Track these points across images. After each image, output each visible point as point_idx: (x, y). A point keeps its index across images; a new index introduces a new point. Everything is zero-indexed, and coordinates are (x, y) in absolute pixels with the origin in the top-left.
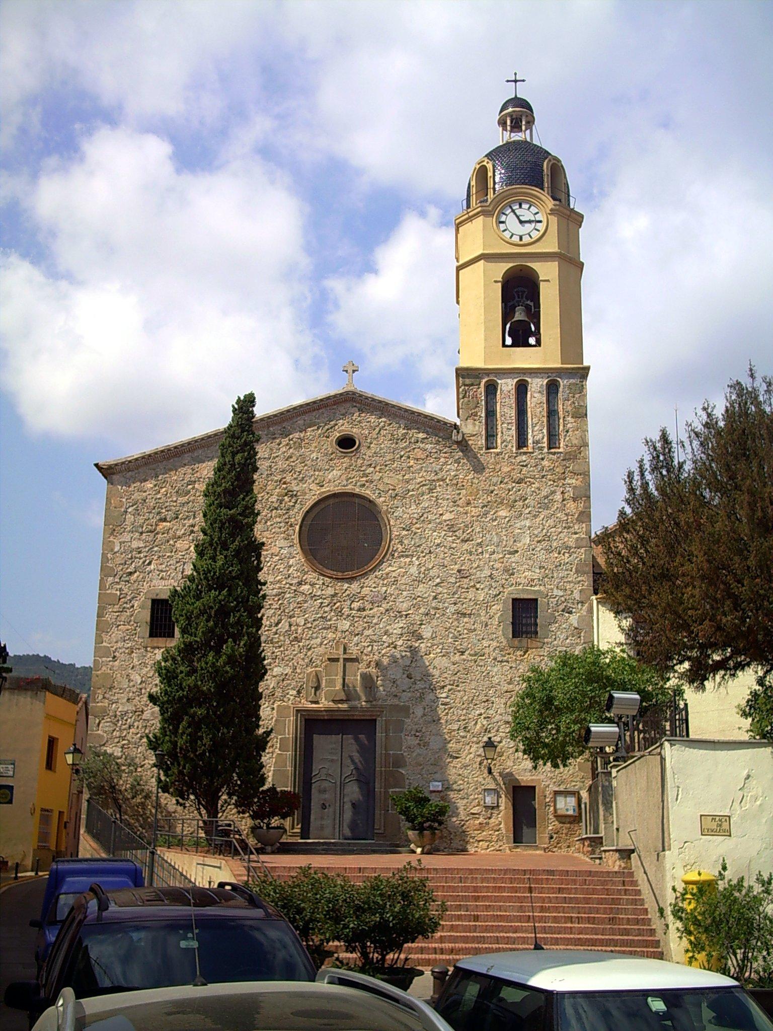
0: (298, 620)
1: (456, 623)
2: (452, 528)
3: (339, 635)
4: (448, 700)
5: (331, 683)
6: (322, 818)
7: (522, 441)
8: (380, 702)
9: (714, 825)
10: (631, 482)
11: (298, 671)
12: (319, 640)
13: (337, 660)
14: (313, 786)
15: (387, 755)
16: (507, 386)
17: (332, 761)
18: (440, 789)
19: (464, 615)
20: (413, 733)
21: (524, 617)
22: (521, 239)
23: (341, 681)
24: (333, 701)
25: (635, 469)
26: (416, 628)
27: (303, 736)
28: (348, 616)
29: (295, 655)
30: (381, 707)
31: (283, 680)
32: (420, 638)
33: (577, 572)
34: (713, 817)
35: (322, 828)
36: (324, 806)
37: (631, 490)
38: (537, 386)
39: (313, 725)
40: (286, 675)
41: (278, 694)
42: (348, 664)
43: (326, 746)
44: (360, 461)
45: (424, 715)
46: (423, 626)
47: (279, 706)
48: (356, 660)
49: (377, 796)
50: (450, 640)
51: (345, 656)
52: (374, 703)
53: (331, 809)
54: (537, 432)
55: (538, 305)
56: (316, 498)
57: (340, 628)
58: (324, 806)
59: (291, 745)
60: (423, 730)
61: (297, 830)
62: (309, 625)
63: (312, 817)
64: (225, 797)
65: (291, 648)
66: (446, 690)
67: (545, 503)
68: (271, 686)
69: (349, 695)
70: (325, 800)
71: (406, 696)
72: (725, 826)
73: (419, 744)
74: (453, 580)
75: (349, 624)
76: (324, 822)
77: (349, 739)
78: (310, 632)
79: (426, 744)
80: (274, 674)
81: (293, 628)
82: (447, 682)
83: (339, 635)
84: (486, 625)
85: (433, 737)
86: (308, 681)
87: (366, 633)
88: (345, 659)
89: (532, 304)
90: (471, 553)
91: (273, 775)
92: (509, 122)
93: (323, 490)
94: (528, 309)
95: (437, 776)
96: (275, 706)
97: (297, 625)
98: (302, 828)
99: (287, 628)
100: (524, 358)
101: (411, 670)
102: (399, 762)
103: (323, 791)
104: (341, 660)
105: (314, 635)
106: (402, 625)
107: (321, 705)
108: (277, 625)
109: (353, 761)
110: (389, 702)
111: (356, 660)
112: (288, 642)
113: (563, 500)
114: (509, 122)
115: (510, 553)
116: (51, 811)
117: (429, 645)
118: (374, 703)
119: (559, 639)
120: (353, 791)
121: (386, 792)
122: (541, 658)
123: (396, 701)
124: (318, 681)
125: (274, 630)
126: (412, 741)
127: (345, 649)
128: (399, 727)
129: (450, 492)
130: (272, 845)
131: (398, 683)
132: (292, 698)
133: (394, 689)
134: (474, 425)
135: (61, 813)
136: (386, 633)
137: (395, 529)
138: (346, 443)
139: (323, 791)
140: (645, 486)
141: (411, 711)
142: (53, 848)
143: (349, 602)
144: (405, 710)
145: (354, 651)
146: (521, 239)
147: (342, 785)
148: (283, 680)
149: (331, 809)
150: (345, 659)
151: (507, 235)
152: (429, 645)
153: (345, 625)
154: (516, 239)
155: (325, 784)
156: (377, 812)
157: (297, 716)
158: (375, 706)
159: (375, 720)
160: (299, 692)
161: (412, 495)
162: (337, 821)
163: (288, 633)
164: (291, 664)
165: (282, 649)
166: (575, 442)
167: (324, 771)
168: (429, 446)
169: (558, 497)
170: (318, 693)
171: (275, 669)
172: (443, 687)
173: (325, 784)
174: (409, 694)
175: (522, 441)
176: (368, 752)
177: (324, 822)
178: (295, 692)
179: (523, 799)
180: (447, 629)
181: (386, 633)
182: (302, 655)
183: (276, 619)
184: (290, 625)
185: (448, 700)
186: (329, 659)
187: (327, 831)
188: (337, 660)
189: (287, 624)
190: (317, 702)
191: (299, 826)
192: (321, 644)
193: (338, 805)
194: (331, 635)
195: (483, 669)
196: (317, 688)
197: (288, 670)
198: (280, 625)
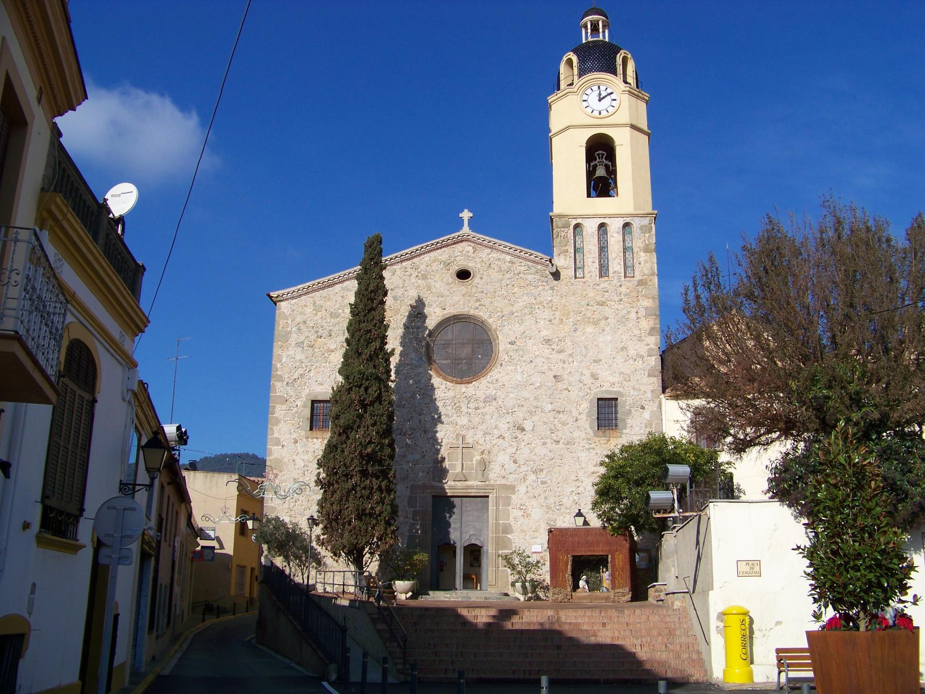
2: (548, 341)
7: (603, 270)
8: (492, 482)
9: (747, 569)
10: (686, 294)
16: (591, 227)
18: (540, 550)
19: (559, 412)
21: (607, 412)
22: (600, 113)
25: (690, 283)
30: (493, 485)
33: (649, 376)
34: (747, 562)
37: (686, 301)
38: (615, 226)
44: (474, 290)
54: (616, 265)
55: (614, 165)
56: (440, 319)
57: (460, 423)
64: (368, 555)
67: (623, 321)
72: (757, 569)
74: (550, 385)
79: (528, 516)
84: (577, 420)
89: (610, 164)
90: (564, 362)
92: (589, 26)
93: (445, 312)
94: (607, 167)
100: (602, 205)
101: (516, 456)
110: (499, 482)
113: (638, 318)
114: (589, 26)
115: (595, 361)
116: (245, 567)
119: (634, 431)
122: (615, 443)
123: (504, 482)
126: (519, 513)
128: (508, 501)
129: (547, 314)
134: (565, 259)
135: (252, 569)
137: (502, 345)
138: (464, 275)
140: (698, 297)
142: (247, 595)
143: (466, 402)
144: (512, 489)
146: (600, 113)
151: (589, 110)
153: (463, 421)
154: (596, 113)
161: (517, 316)
166: (646, 272)
168: (530, 277)
169: (633, 316)
174: (516, 476)
175: (603, 270)
195: (574, 455)
197: (418, 456)
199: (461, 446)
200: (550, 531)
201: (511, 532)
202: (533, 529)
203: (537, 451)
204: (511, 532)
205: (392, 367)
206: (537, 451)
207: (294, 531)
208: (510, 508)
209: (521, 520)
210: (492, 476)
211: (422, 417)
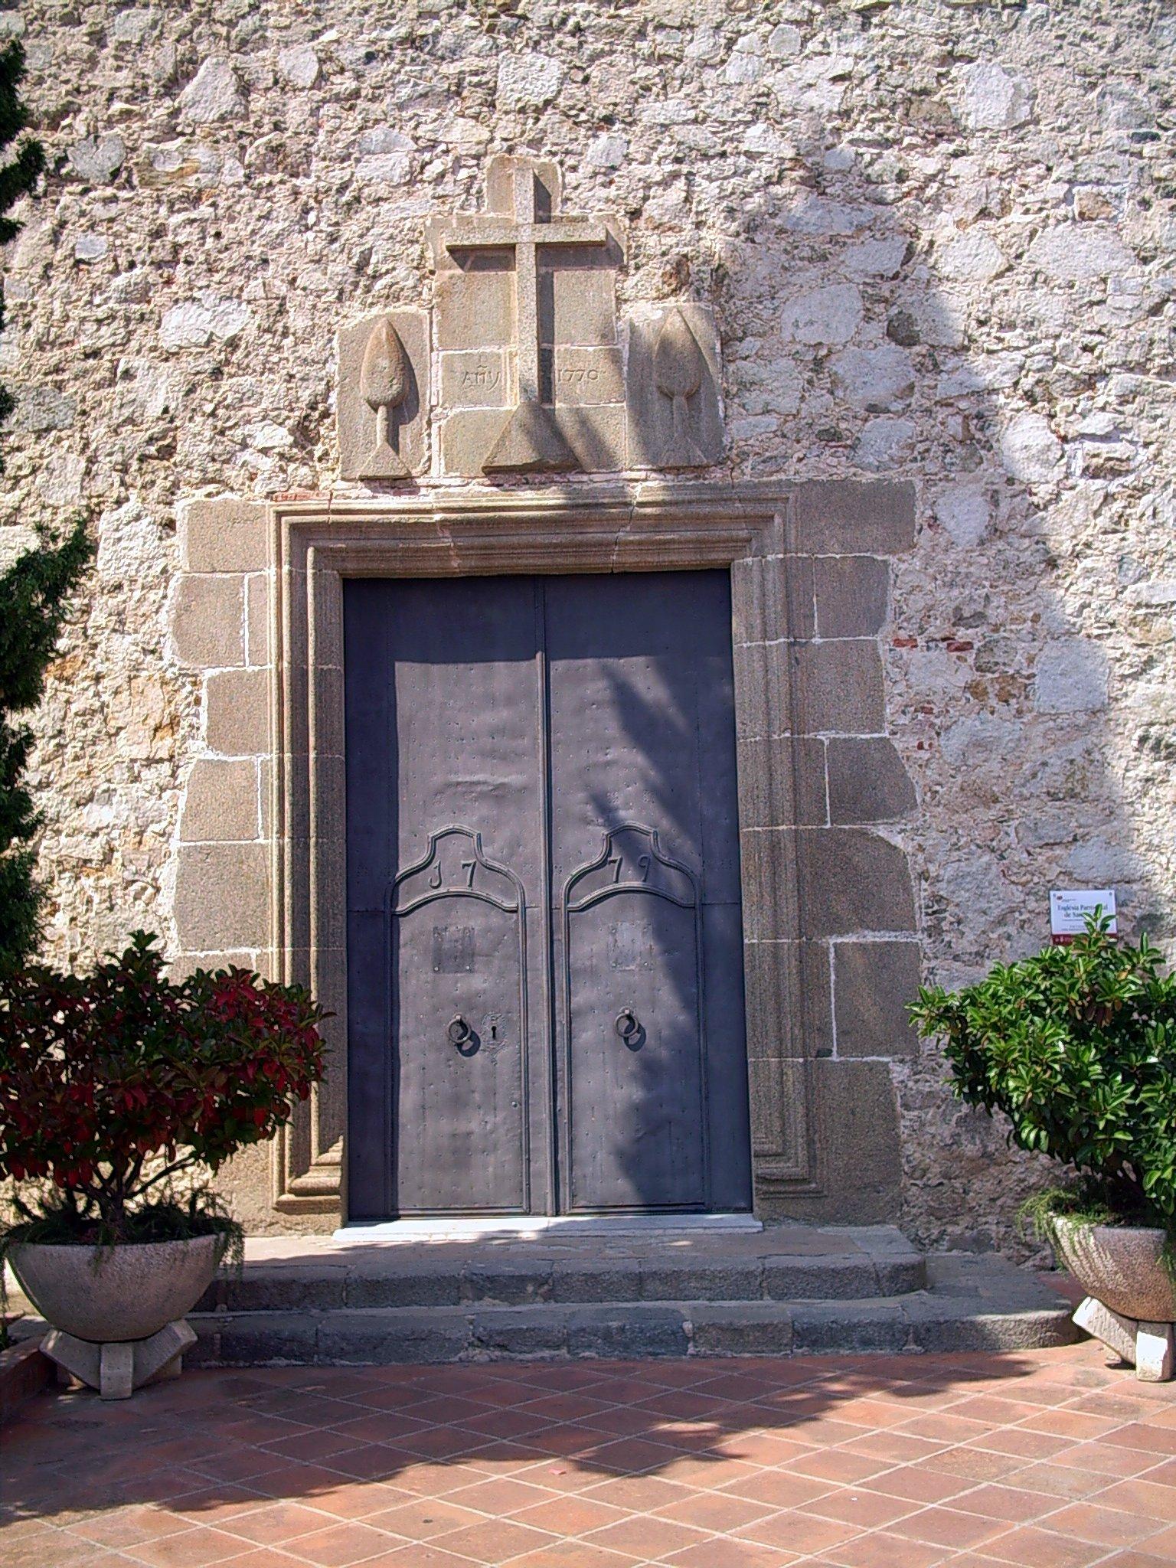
0: (286, 61)
1: (1136, 47)
3: (507, 127)
4: (1120, 449)
5: (473, 376)
6: (458, 1103)
8: (747, 473)
11: (297, 321)
12: (398, 162)
13: (500, 257)
14: (407, 929)
15: (803, 752)
17: (499, 794)
20: (937, 627)
23: (527, 365)
24: (495, 473)
26: (922, 75)
27: (336, 666)
28: (551, 29)
29: (276, 243)
30: (756, 495)
31: (217, 373)
32: (945, 130)
35: (460, 1153)
36: (465, 1039)
39: (388, 610)
40: (233, 344)
41: (194, 442)
42: (565, 280)
43: (459, 716)
45: (996, 532)
46: (958, 70)
47: (197, 509)
48: (598, 254)
49: (750, 774)
50: (1112, 135)
51: (552, 234)
52: (717, 475)
53: (507, 1052)
57: (509, 95)
58: (465, 1039)
59: (268, 715)
60: (994, 614)
61: (325, 1175)
62: (345, 84)
63: (408, 1099)
65: (251, 209)
66: (1107, 392)
68: (154, 409)
69: (556, 449)
70: (469, 1002)
71: (884, 438)
73: (975, 690)
75: (555, 68)
76: (473, 1123)
77: (583, 682)
78: (353, 121)
79: (1014, 689)
80: (169, 340)
81: (258, 103)
82: (1111, 353)
83: (507, 127)
85: (1051, 650)
86: (350, 372)
87: (652, 111)
88: (551, 255)
91: (182, 878)
95: (1087, 857)
96: (179, 511)
97: (282, 84)
98: (352, 1165)
99: (228, 100)
102: (869, 786)
103: (453, 957)
104: (526, 258)
105: (376, 134)
106: (844, 66)
107: (425, 499)
108: (172, 85)
109: (604, 808)
110: (795, 471)
111: (598, 254)
112: (233, 172)
117: (1001, 162)
118: (717, 475)
120: (621, 949)
121: (809, 957)
123: (833, 465)
124: (406, 369)
125: (160, 113)
126: (939, 674)
127: (543, 200)
128: (864, 600)
130: (138, 1340)
131: (839, 366)
132: (267, 464)
133: (819, 402)
136: (761, 107)
139: (453, 957)
141: (921, 513)
144: (889, 510)
145: (590, 211)
147: (559, 926)
148: (217, 373)
149: (507, 1052)
150: (551, 255)
152: (1001, 162)
155: (470, 920)
156: (763, 1063)
157: (298, 561)
158: (721, 495)
159: (722, 574)
160: (304, 435)
162: (542, 1114)
163: (232, 128)
164: (254, 288)
165: (204, 210)
167: (456, 851)
170: (406, 433)
171: (173, 319)
172: (1090, 381)
173: (470, 920)
174: (907, 427)
176: (693, 752)
177: (473, 1123)
178: (280, 437)
179: (637, 268)
180: (1091, 80)
181: (761, 107)
182: (313, 241)
183: (164, 58)
184: (245, 89)
185: (1120, 449)
186: (461, 254)
187: (492, 1168)
188: (500, 257)
189: (227, 81)
190: (401, 484)
191: (336, 1153)
192: (412, 180)
193: (540, 1025)
194: (462, 133)
196: (402, 407)
197: (240, 321)
198: (189, 89)
199: (528, 236)
200: (302, 534)
201: (898, 802)
202: (1053, 777)
203: (1046, 251)
204: (898, 802)
205: (416, 1310)
206: (1046, 251)
207: (84, 572)
208: (882, 640)
209: (967, 725)
210: (744, 428)
211: (256, 62)
